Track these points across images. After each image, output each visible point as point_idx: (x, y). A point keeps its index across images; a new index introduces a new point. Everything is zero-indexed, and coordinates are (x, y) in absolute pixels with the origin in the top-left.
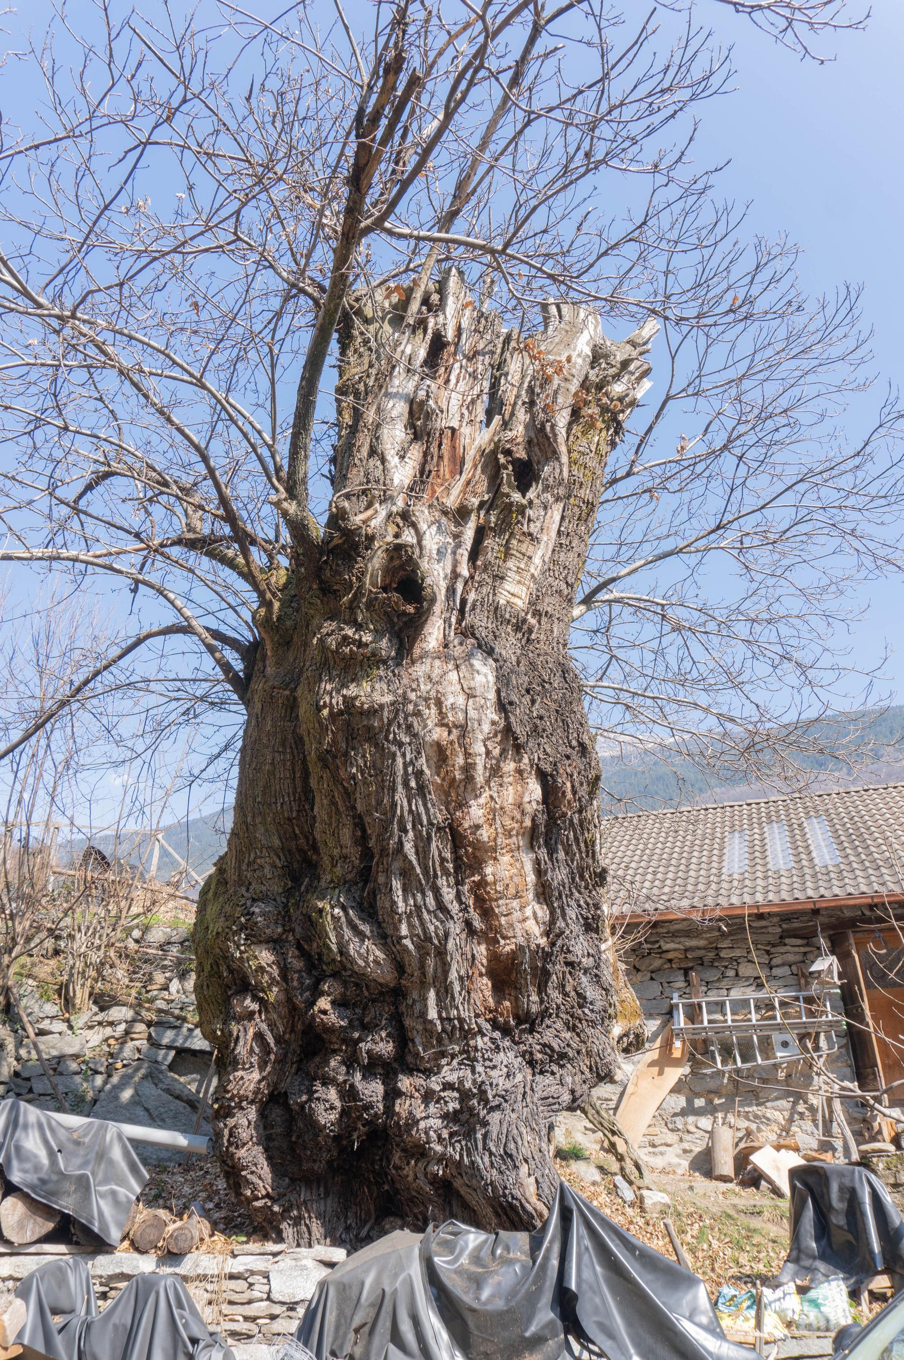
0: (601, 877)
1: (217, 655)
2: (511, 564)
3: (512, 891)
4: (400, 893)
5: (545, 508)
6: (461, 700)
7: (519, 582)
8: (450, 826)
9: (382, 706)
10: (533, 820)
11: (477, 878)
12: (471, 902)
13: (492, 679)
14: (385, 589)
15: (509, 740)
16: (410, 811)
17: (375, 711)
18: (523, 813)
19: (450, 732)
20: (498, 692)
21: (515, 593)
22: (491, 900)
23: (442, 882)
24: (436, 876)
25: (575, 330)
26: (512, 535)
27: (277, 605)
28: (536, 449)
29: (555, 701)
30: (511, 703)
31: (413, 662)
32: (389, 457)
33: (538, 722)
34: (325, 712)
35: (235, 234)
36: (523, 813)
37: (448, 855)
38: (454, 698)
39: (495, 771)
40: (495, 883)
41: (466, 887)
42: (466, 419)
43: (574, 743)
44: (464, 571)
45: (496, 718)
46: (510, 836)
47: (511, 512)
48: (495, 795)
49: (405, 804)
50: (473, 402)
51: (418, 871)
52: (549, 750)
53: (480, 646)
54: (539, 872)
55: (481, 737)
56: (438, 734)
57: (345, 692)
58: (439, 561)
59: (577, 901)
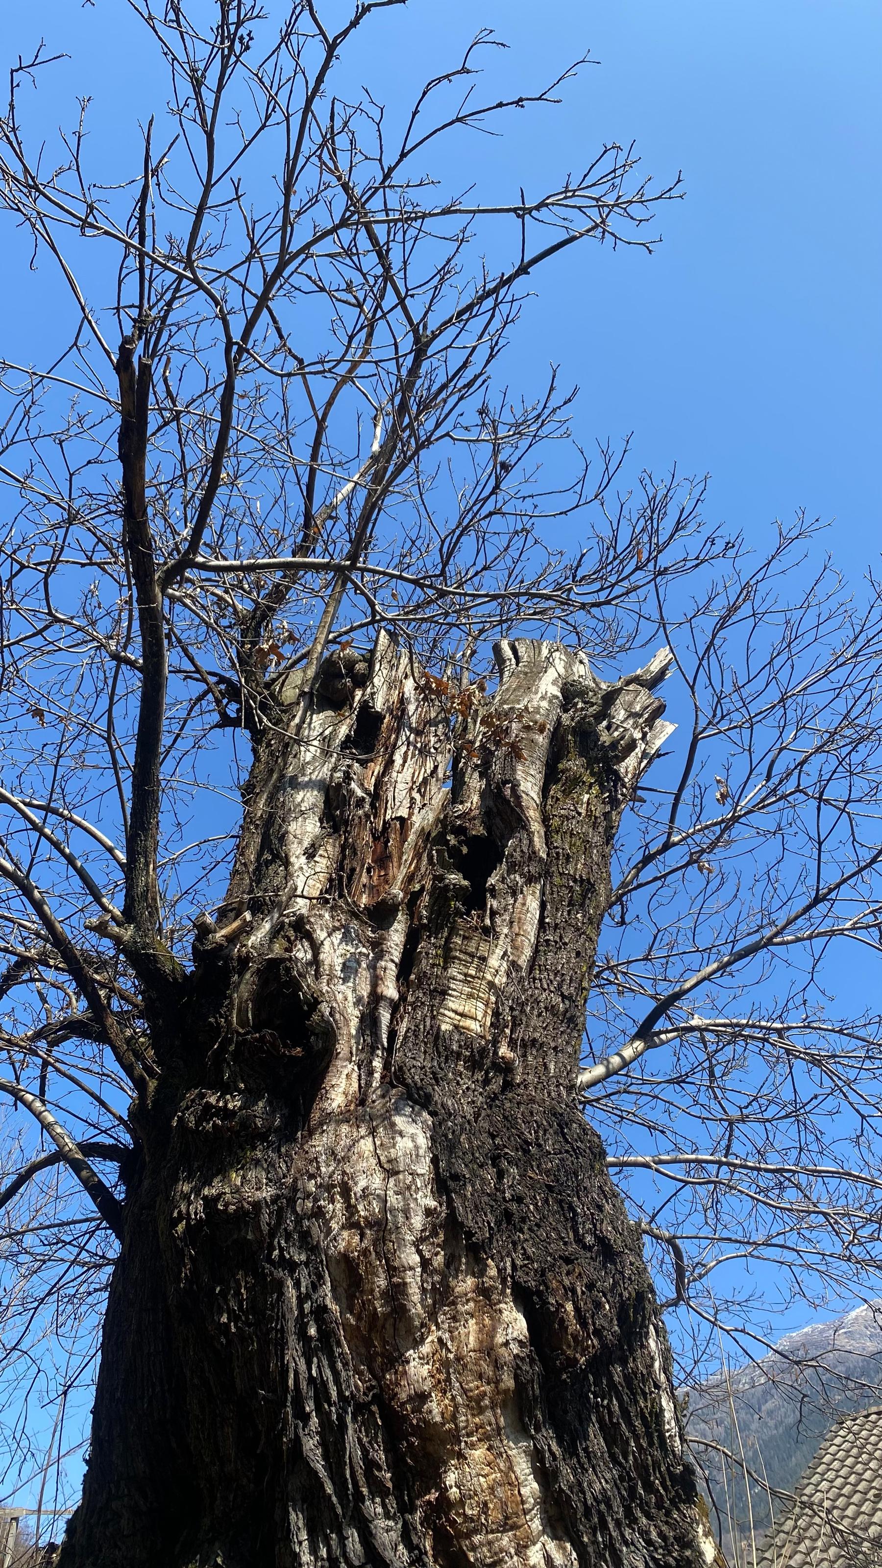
0: (684, 1485)
1: (84, 1173)
2: (453, 971)
3: (495, 1515)
4: (304, 1536)
5: (514, 894)
6: (377, 1182)
7: (470, 996)
8: (377, 1399)
9: (257, 1205)
10: (516, 1377)
11: (433, 1496)
12: (428, 1545)
13: (423, 1141)
14: (257, 1028)
15: (457, 1239)
16: (311, 1380)
17: (248, 1214)
18: (497, 1365)
19: (362, 1236)
20: (435, 1161)
21: (466, 1011)
22: (461, 1535)
23: (373, 1508)
24: (359, 1498)
25: (536, 670)
26: (453, 931)
27: (152, 1084)
28: (498, 820)
29: (548, 1172)
30: (456, 1177)
31: (311, 1133)
32: (293, 859)
33: (514, 1206)
34: (181, 1228)
35: (50, 613)
36: (497, 1365)
37: (381, 1456)
38: (368, 1179)
39: (441, 1296)
40: (461, 1503)
41: (418, 1515)
42: (419, 803)
43: (589, 1239)
44: (390, 990)
45: (432, 1204)
46: (481, 1411)
47: (448, 900)
48: (446, 1336)
49: (302, 1367)
50: (425, 781)
51: (329, 1489)
52: (530, 1251)
53: (410, 1097)
54: (545, 1475)
55: (409, 1238)
56: (347, 1241)
57: (206, 1191)
58: (345, 980)
59: (645, 1534)
